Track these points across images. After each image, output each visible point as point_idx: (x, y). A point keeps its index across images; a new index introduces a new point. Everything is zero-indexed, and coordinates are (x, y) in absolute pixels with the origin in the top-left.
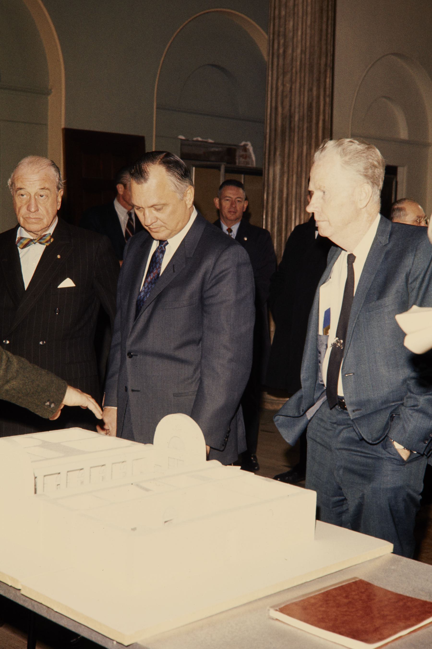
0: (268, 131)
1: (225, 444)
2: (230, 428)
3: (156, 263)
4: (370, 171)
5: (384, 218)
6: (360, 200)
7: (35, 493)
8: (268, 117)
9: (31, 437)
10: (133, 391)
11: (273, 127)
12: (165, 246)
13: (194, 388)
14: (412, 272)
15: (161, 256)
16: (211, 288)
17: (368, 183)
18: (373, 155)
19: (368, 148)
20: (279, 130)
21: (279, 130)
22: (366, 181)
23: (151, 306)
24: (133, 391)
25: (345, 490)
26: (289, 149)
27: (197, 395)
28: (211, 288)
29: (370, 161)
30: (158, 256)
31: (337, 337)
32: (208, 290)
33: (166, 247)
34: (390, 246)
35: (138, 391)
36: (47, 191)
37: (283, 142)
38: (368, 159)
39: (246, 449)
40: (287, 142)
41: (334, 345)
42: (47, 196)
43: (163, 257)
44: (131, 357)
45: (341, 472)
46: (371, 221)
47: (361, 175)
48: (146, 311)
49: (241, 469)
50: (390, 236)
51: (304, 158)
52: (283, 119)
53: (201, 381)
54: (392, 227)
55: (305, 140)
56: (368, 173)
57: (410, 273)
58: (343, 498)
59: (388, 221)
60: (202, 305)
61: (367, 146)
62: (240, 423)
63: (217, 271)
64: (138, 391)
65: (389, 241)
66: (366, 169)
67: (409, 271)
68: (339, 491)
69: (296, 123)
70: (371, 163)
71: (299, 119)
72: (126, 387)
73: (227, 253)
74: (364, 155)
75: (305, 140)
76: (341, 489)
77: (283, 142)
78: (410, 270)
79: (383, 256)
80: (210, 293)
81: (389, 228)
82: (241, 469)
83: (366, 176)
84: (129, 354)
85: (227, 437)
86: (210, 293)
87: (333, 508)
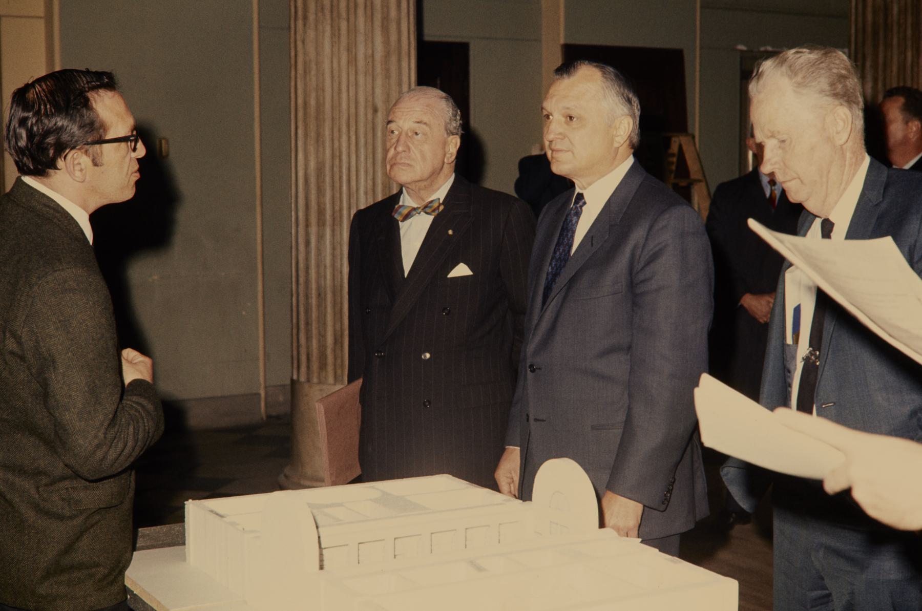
0: (853, 31)
1: (666, 501)
2: (674, 478)
3: (568, 231)
4: (840, 86)
5: (877, 163)
6: (838, 133)
7: (321, 568)
8: (853, 11)
9: (373, 487)
10: (536, 420)
11: (860, 25)
12: (581, 207)
13: (621, 417)
14: (918, 244)
15: (574, 219)
16: (643, 269)
17: (841, 105)
18: (837, 62)
19: (826, 54)
20: (869, 29)
21: (869, 29)
22: (837, 102)
23: (563, 293)
24: (536, 420)
25: (827, 582)
26: (885, 57)
27: (625, 428)
28: (643, 269)
29: (835, 71)
30: (571, 221)
31: (810, 346)
32: (638, 273)
33: (584, 208)
34: (884, 206)
35: (543, 421)
36: (424, 126)
37: (876, 47)
38: (830, 69)
39: (709, 514)
40: (881, 48)
41: (807, 360)
42: (425, 134)
43: (577, 222)
44: (533, 371)
45: (821, 553)
46: (857, 164)
47: (827, 96)
48: (552, 304)
49: (642, 542)
50: (885, 189)
51: (909, 71)
52: (875, 13)
53: (630, 409)
54: (888, 177)
55: (909, 43)
56: (838, 91)
57: (915, 246)
58: (827, 592)
59: (884, 167)
60: (634, 292)
61: (823, 52)
62: (699, 473)
63: (651, 245)
64: (543, 421)
65: (883, 197)
66: (832, 84)
67: (913, 242)
68: (819, 581)
69: (895, 18)
70: (837, 74)
71: (900, 12)
72: (528, 415)
73: (667, 216)
74: (823, 65)
75: (909, 43)
76: (822, 579)
77: (876, 47)
78: (916, 241)
79: (874, 221)
80: (641, 277)
81: (884, 177)
82: (642, 542)
83: (836, 95)
84: (531, 366)
85: (670, 491)
86: (641, 277)
87: (812, 607)
